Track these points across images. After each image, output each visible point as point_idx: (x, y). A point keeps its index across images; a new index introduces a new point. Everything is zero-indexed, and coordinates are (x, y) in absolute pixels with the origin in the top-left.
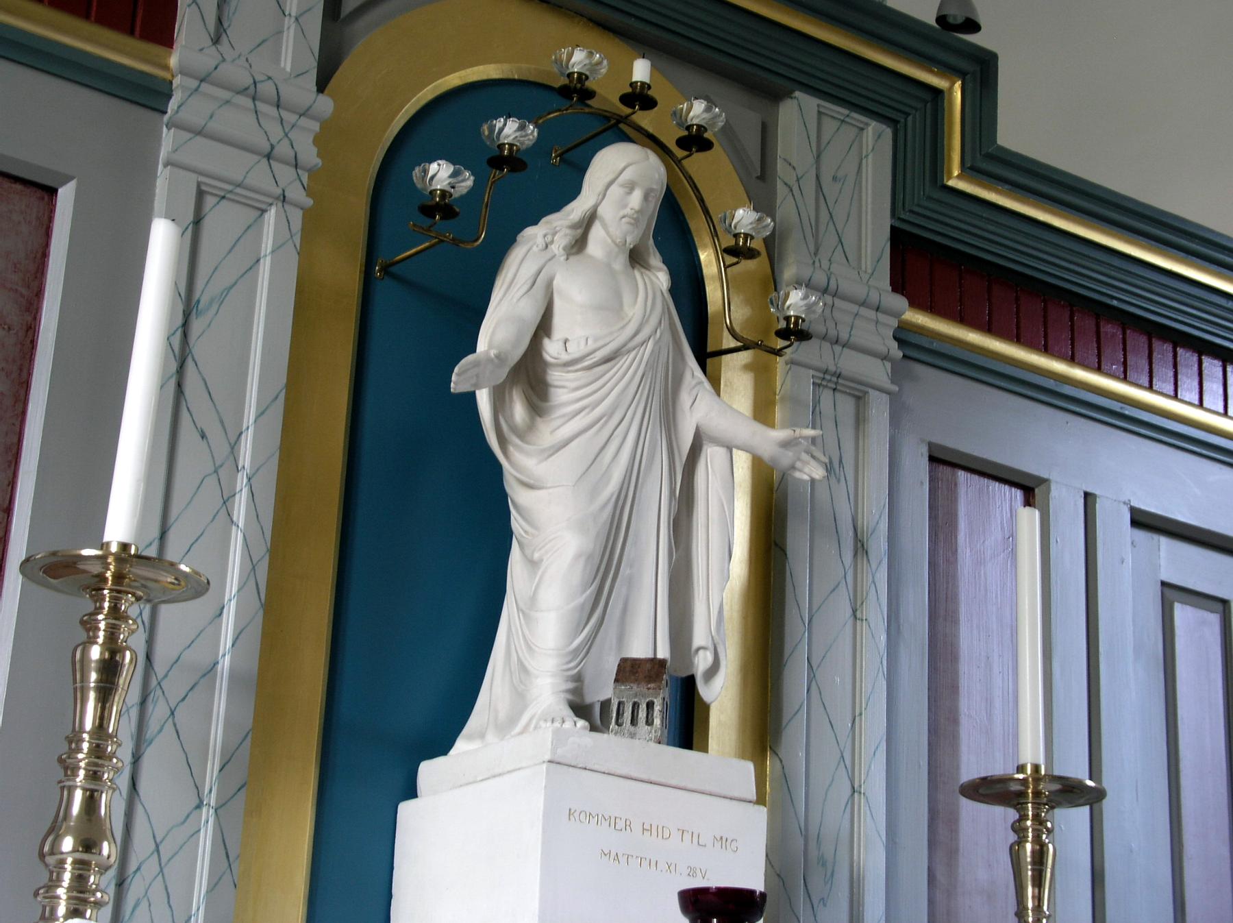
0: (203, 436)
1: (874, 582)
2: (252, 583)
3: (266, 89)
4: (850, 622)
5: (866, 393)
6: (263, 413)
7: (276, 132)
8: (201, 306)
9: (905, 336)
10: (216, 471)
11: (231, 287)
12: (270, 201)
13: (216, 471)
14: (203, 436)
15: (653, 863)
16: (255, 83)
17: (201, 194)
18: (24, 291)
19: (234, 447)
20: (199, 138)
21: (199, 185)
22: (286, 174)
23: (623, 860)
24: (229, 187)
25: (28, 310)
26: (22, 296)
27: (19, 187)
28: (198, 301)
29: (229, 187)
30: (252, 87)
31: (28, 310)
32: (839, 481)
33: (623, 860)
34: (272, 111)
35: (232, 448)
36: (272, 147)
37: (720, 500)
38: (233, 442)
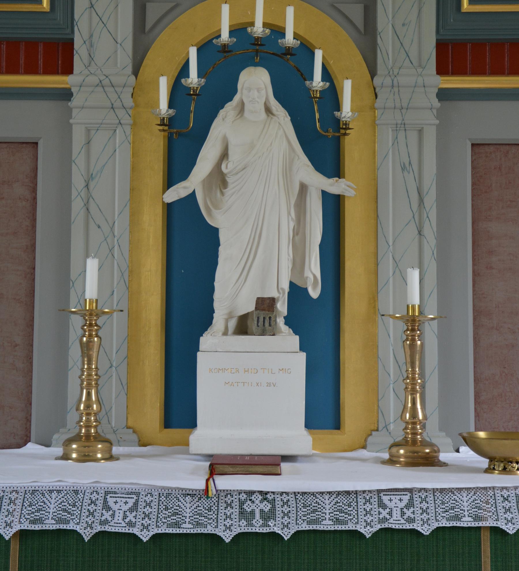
0: (99, 227)
1: (428, 217)
2: (122, 280)
3: (106, 82)
4: (417, 237)
5: (423, 128)
6: (120, 213)
7: (113, 97)
8: (93, 176)
9: (444, 95)
10: (105, 240)
11: (104, 166)
12: (116, 126)
13: (105, 240)
14: (99, 227)
15: (250, 384)
16: (101, 81)
17: (88, 131)
18: (31, 185)
19: (112, 228)
20: (102, 88)
21: (86, 127)
22: (121, 113)
23: (236, 384)
24: (98, 126)
25: (33, 192)
26: (31, 187)
27: (24, 145)
28: (92, 174)
29: (98, 126)
30: (100, 84)
31: (33, 192)
32: (409, 173)
33: (236, 384)
34: (112, 89)
35: (112, 229)
36: (112, 104)
37: (294, 227)
38: (111, 226)
